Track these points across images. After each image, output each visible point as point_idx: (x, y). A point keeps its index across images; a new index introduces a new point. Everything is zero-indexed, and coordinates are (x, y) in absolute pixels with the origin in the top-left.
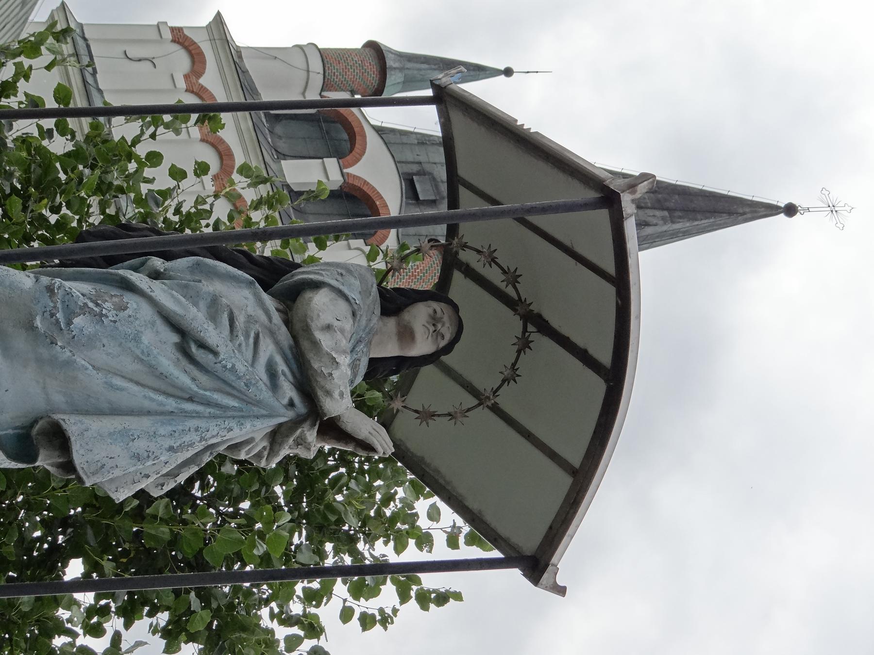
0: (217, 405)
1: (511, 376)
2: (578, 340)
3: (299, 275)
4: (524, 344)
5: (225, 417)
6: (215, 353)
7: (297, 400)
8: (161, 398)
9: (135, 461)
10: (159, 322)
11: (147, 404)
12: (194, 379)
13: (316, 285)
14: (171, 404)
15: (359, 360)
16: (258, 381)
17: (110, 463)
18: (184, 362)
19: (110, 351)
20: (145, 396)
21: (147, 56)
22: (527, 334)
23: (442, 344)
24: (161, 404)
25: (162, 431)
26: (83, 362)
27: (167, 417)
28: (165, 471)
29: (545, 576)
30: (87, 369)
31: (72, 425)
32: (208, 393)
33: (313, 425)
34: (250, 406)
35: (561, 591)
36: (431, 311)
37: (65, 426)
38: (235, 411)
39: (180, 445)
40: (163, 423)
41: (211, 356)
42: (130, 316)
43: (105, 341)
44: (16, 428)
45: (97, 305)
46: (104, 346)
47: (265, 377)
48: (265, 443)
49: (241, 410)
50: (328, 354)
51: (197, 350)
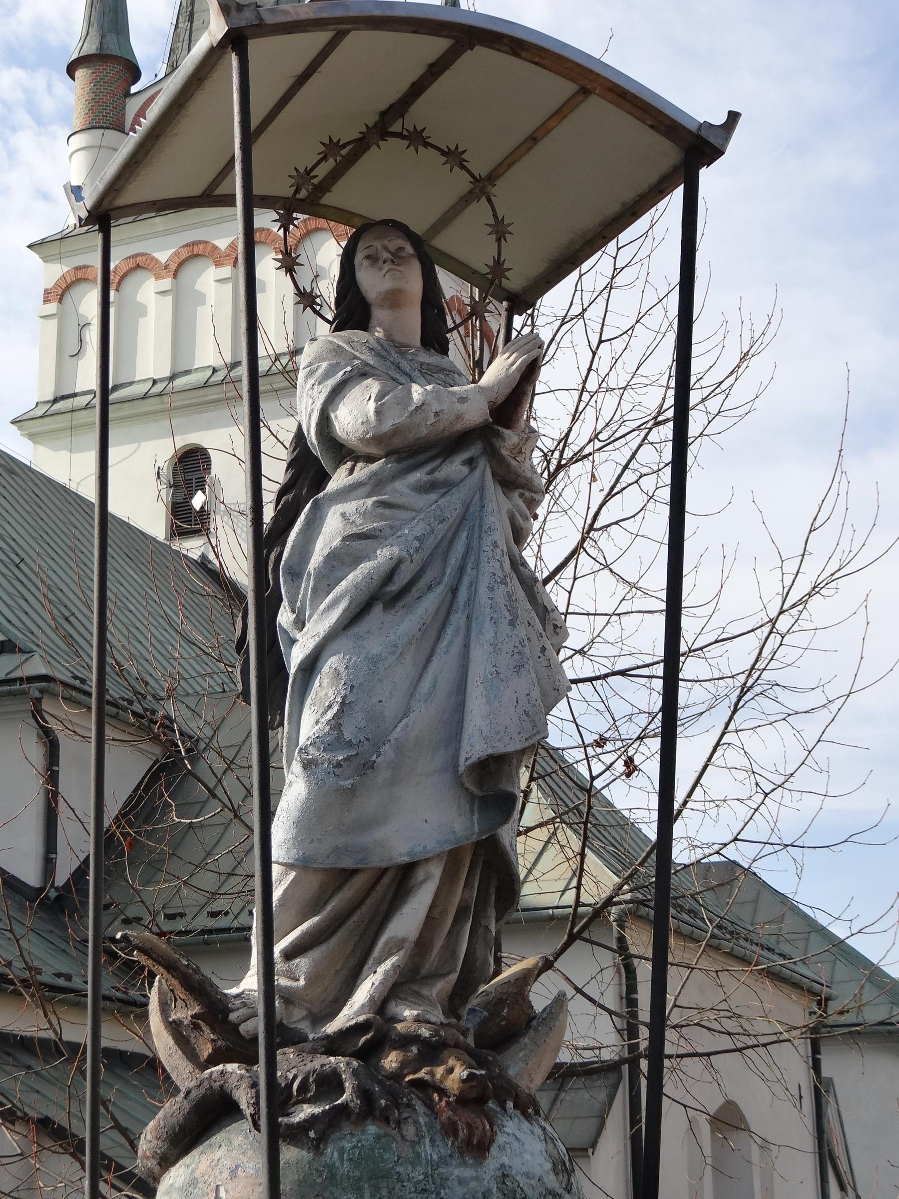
0: (465, 557)
1: (454, 157)
2: (415, 74)
3: (312, 436)
4: (417, 138)
5: (479, 549)
7: (466, 455)
8: (450, 630)
9: (523, 672)
10: (358, 629)
11: (456, 649)
12: (430, 588)
14: (458, 619)
15: (422, 364)
16: (439, 507)
17: (523, 702)
18: (408, 599)
19: (387, 693)
20: (446, 652)
21: (77, 333)
22: (405, 133)
23: (410, 250)
24: (457, 632)
25: (489, 635)
26: (398, 729)
27: (474, 625)
28: (539, 627)
29: (711, 139)
30: (407, 725)
31: (474, 747)
32: (448, 571)
33: (499, 435)
34: (469, 519)
35: (734, 117)
36: (366, 263)
37: (474, 759)
38: (472, 534)
39: (509, 611)
40: (480, 632)
41: (403, 567)
42: (347, 668)
43: (375, 700)
44: (472, 812)
45: (330, 707)
46: (381, 701)
47: (433, 496)
48: (516, 494)
49: (472, 528)
50: (411, 415)
51: (394, 583)
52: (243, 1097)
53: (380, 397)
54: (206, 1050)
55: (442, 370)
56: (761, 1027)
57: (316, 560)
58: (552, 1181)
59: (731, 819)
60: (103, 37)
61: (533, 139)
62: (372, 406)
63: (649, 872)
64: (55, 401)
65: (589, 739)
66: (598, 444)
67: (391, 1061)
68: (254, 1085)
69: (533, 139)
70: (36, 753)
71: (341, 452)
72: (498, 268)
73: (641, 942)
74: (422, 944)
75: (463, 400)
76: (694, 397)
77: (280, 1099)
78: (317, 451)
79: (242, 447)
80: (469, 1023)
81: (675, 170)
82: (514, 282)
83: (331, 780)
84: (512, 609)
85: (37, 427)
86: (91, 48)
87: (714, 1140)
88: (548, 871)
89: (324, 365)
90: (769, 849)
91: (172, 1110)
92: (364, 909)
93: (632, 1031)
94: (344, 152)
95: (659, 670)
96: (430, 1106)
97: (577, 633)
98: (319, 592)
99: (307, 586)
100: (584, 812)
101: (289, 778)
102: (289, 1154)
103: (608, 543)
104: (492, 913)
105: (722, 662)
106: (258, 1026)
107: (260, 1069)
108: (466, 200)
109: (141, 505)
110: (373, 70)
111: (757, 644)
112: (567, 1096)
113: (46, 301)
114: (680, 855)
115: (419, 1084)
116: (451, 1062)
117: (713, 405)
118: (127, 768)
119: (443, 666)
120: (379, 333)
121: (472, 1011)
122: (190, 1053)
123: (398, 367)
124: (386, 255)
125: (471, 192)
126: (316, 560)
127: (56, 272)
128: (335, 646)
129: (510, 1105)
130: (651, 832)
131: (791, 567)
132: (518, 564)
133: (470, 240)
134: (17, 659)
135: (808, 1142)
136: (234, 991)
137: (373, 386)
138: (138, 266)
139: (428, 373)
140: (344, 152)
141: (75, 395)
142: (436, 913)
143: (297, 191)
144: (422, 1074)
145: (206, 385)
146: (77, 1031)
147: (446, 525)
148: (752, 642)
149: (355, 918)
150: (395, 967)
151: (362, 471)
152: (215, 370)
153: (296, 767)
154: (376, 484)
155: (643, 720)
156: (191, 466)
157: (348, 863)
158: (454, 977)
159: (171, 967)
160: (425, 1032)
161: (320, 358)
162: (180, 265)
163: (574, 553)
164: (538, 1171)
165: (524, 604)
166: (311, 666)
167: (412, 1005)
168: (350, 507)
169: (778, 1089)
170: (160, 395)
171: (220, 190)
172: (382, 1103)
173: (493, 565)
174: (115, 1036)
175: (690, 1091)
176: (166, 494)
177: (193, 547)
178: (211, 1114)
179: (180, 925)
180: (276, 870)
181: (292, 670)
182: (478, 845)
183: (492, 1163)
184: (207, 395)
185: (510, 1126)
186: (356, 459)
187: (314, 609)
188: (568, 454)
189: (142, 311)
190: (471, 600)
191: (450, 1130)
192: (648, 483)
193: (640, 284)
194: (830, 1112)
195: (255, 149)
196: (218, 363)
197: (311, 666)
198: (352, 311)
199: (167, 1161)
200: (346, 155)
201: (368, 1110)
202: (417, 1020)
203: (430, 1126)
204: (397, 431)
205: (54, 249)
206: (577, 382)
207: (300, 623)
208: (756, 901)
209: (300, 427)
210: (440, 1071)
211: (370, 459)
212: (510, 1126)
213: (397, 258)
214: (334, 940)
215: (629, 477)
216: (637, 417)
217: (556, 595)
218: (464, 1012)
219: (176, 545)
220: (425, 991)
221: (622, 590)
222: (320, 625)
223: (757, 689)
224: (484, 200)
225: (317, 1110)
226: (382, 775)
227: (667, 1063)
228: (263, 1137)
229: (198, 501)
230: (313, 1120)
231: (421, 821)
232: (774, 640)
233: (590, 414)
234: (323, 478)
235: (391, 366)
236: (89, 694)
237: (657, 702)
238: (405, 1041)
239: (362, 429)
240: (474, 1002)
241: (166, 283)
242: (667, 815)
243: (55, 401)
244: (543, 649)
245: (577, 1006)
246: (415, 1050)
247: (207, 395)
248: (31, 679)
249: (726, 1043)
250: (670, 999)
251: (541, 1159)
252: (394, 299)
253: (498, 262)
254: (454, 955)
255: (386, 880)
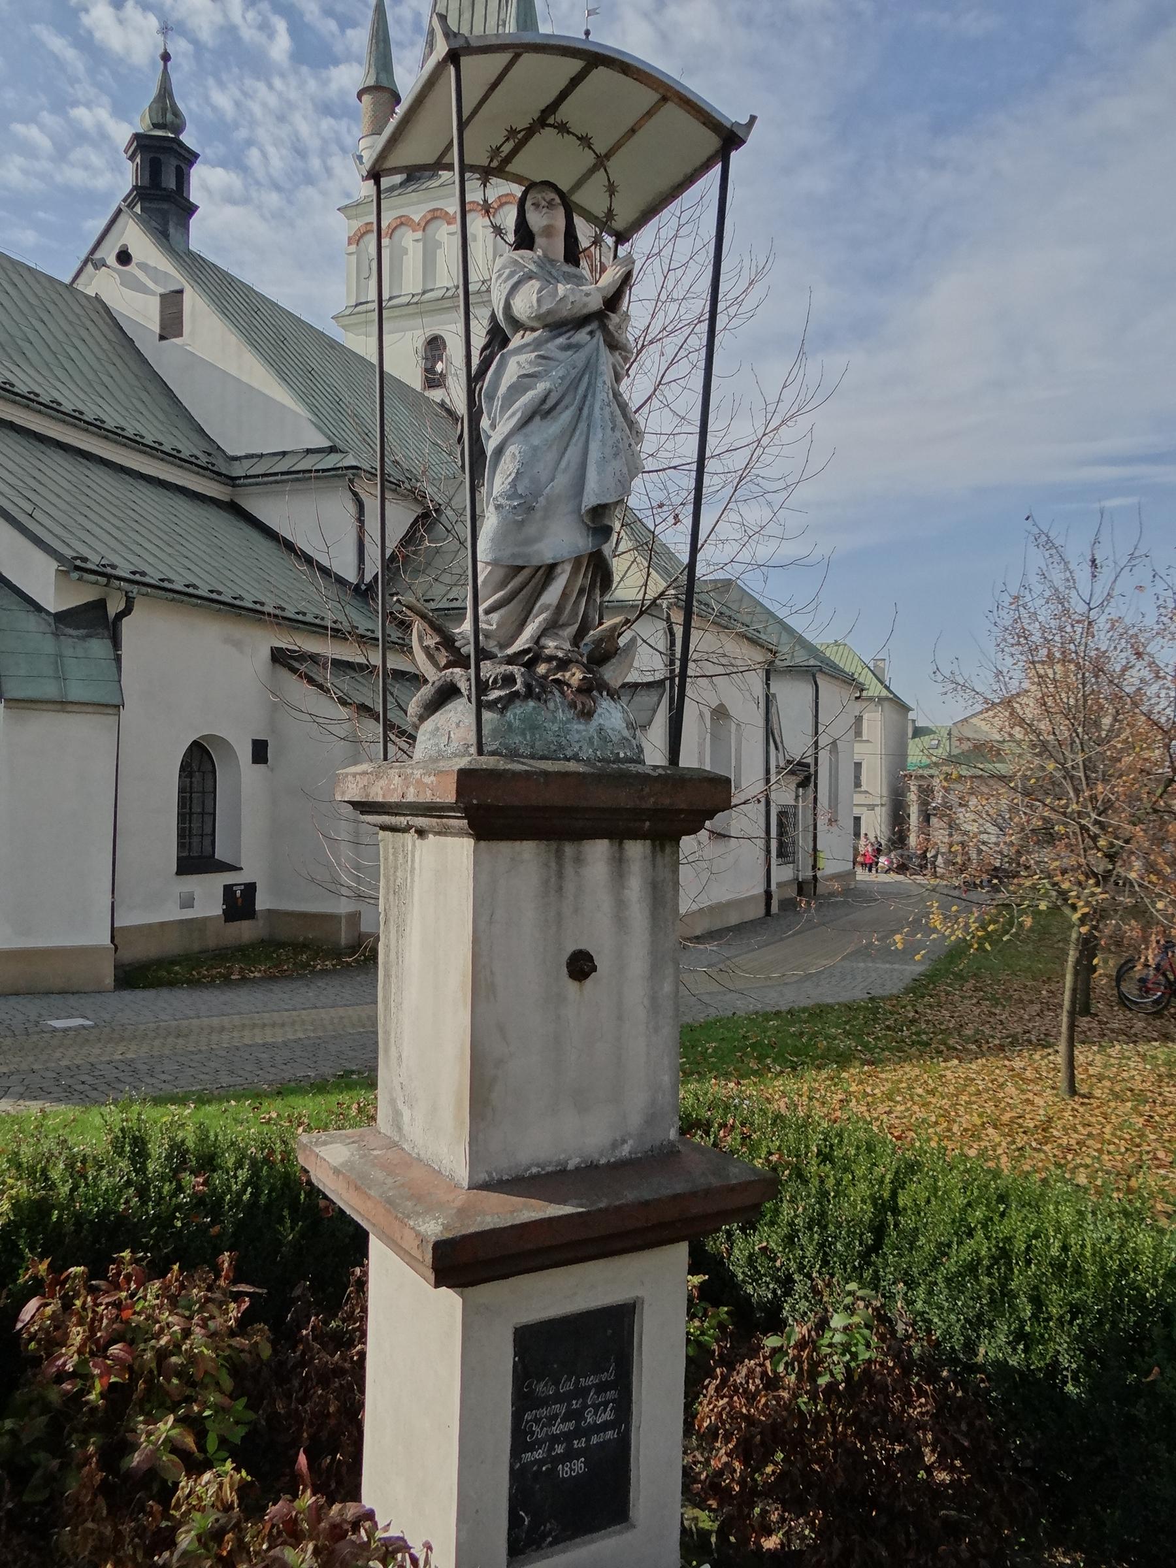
1: (585, 141)
2: (562, 84)
4: (563, 128)
6: (550, 391)
7: (588, 329)
10: (524, 431)
11: (580, 445)
12: (567, 408)
13: (508, 307)
14: (582, 426)
18: (554, 413)
23: (558, 200)
24: (581, 434)
31: (590, 499)
33: (607, 317)
34: (590, 367)
35: (753, 119)
36: (532, 208)
47: (569, 353)
52: (463, 686)
53: (540, 291)
54: (443, 662)
55: (575, 276)
56: (739, 662)
57: (502, 390)
58: (626, 733)
59: (730, 550)
60: (378, 74)
61: (633, 131)
62: (535, 297)
63: (684, 578)
64: (356, 306)
65: (654, 504)
66: (665, 333)
67: (542, 669)
68: (469, 680)
69: (633, 131)
70: (352, 508)
71: (517, 325)
72: (610, 214)
73: (678, 617)
74: (559, 608)
75: (587, 295)
76: (721, 306)
77: (482, 687)
78: (503, 325)
79: (460, 327)
80: (585, 650)
81: (717, 152)
82: (619, 224)
83: (511, 515)
84: (613, 421)
85: (346, 321)
86: (371, 82)
87: (712, 719)
88: (630, 580)
89: (507, 271)
90: (750, 567)
91: (426, 692)
92: (528, 588)
93: (672, 663)
94: (519, 136)
95: (694, 467)
96: (562, 693)
97: (648, 445)
98: (505, 407)
99: (497, 403)
100: (650, 547)
101: (487, 514)
102: (487, 715)
103: (670, 392)
104: (598, 592)
105: (729, 462)
106: (470, 649)
107: (472, 671)
108: (592, 170)
109: (405, 367)
110: (539, 79)
111: (750, 453)
112: (636, 699)
113: (350, 244)
114: (700, 570)
115: (557, 681)
116: (574, 670)
117: (732, 311)
118: (401, 517)
119: (573, 454)
120: (540, 252)
121: (586, 645)
122: (435, 664)
123: (550, 273)
124: (544, 203)
125: (595, 165)
126: (502, 390)
127: (357, 224)
128: (513, 440)
129: (605, 693)
130: (685, 559)
131: (771, 408)
132: (617, 395)
133: (592, 197)
134: (338, 456)
135: (761, 723)
136: (457, 631)
137: (535, 284)
138: (402, 224)
139: (568, 278)
140: (519, 136)
141: (367, 302)
142: (567, 591)
143: (491, 161)
144: (558, 676)
145: (443, 298)
146: (376, 659)
147: (577, 370)
148: (747, 452)
149: (523, 592)
150: (544, 620)
151: (530, 337)
152: (448, 289)
153: (492, 508)
154: (537, 344)
155: (685, 494)
156: (435, 345)
157: (520, 563)
158: (576, 626)
159: (423, 617)
160: (560, 654)
161: (504, 267)
162: (427, 223)
163: (650, 398)
164: (618, 727)
165: (620, 419)
166: (499, 451)
167: (554, 640)
168: (522, 358)
169: (747, 694)
170: (416, 303)
171: (446, 160)
172: (536, 691)
173: (603, 394)
174: (396, 662)
175: (699, 697)
176: (422, 363)
177: (436, 395)
178: (447, 693)
179: (433, 605)
180: (480, 566)
181: (489, 454)
182: (591, 555)
183: (596, 721)
184: (440, 305)
185: (605, 704)
186: (526, 330)
187: (501, 418)
188: (648, 338)
189: (406, 252)
190: (590, 415)
191: (573, 705)
192: (693, 357)
193: (694, 234)
194: (773, 710)
195: (466, 134)
196: (450, 285)
197: (499, 451)
198: (525, 238)
199: (422, 718)
200: (521, 138)
201: (529, 693)
202: (556, 648)
203: (562, 703)
204: (549, 312)
205: (353, 212)
206: (654, 295)
207: (493, 426)
208: (741, 600)
209: (493, 317)
210: (568, 675)
211: (533, 330)
212: (605, 704)
213: (550, 205)
214: (512, 604)
215: (682, 353)
216: (689, 317)
217: (640, 418)
218: (581, 645)
219: (426, 394)
220: (560, 633)
221: (676, 420)
222: (505, 426)
223: (748, 478)
224: (602, 170)
225: (502, 693)
226: (539, 515)
227: (688, 680)
228: (473, 706)
229: (439, 367)
230: (500, 699)
231: (562, 540)
232: (759, 451)
233: (662, 313)
234: (506, 341)
235: (546, 273)
236: (377, 640)
237: (693, 485)
238: (550, 659)
239: (529, 311)
240: (587, 639)
241: (419, 235)
242: (694, 550)
243: (356, 306)
244: (630, 445)
245: (643, 649)
246: (555, 663)
247: (440, 305)
248: (347, 468)
249: (721, 670)
250: (692, 647)
251: (620, 722)
252: (548, 231)
253: (610, 210)
254: (577, 614)
255: (540, 572)
